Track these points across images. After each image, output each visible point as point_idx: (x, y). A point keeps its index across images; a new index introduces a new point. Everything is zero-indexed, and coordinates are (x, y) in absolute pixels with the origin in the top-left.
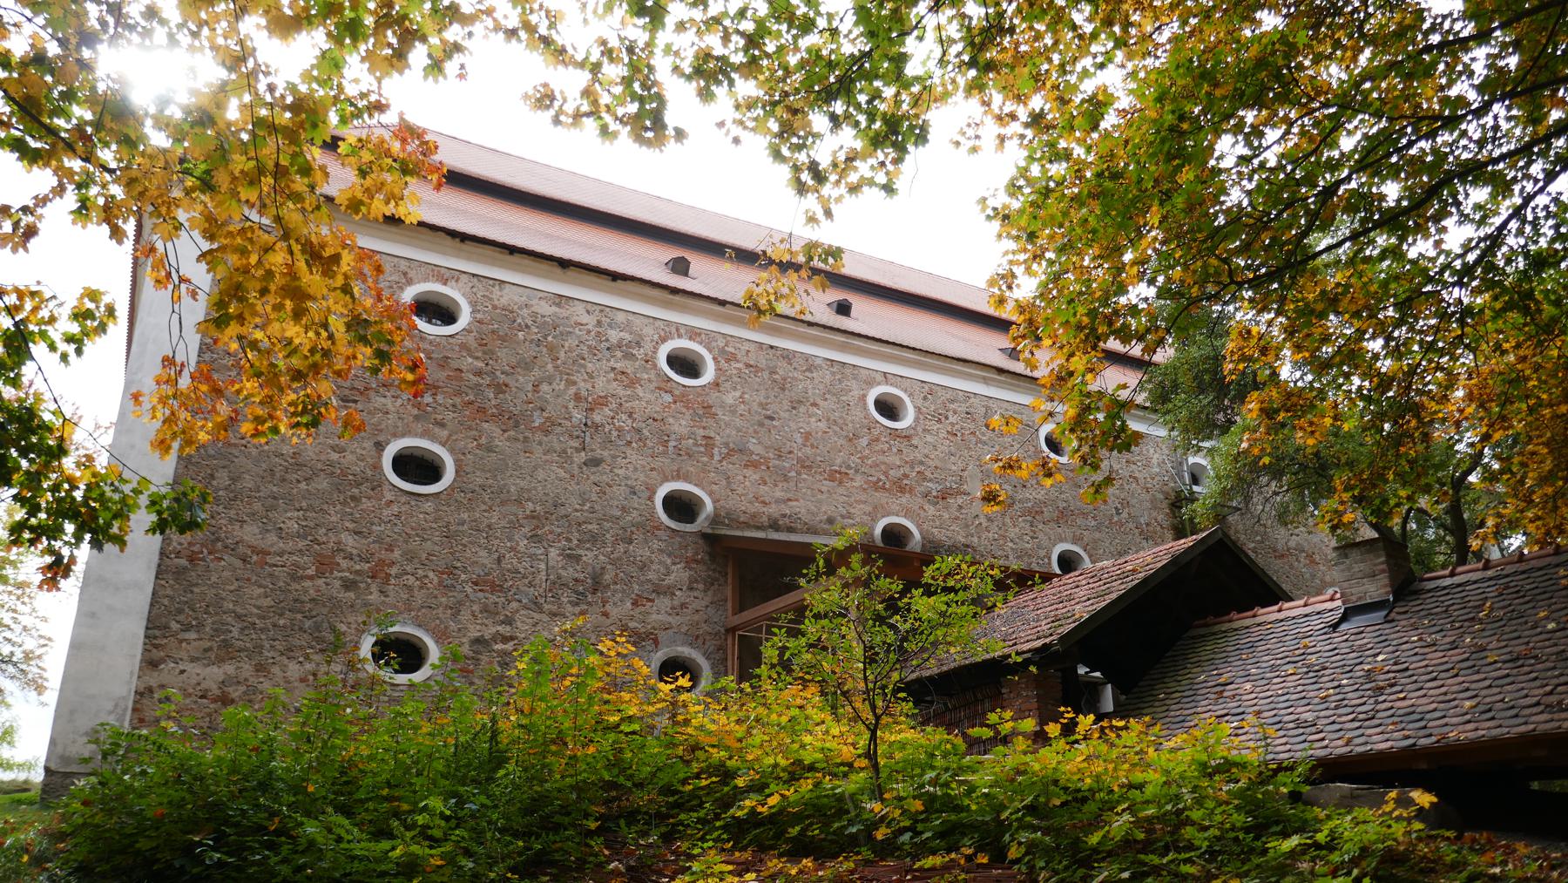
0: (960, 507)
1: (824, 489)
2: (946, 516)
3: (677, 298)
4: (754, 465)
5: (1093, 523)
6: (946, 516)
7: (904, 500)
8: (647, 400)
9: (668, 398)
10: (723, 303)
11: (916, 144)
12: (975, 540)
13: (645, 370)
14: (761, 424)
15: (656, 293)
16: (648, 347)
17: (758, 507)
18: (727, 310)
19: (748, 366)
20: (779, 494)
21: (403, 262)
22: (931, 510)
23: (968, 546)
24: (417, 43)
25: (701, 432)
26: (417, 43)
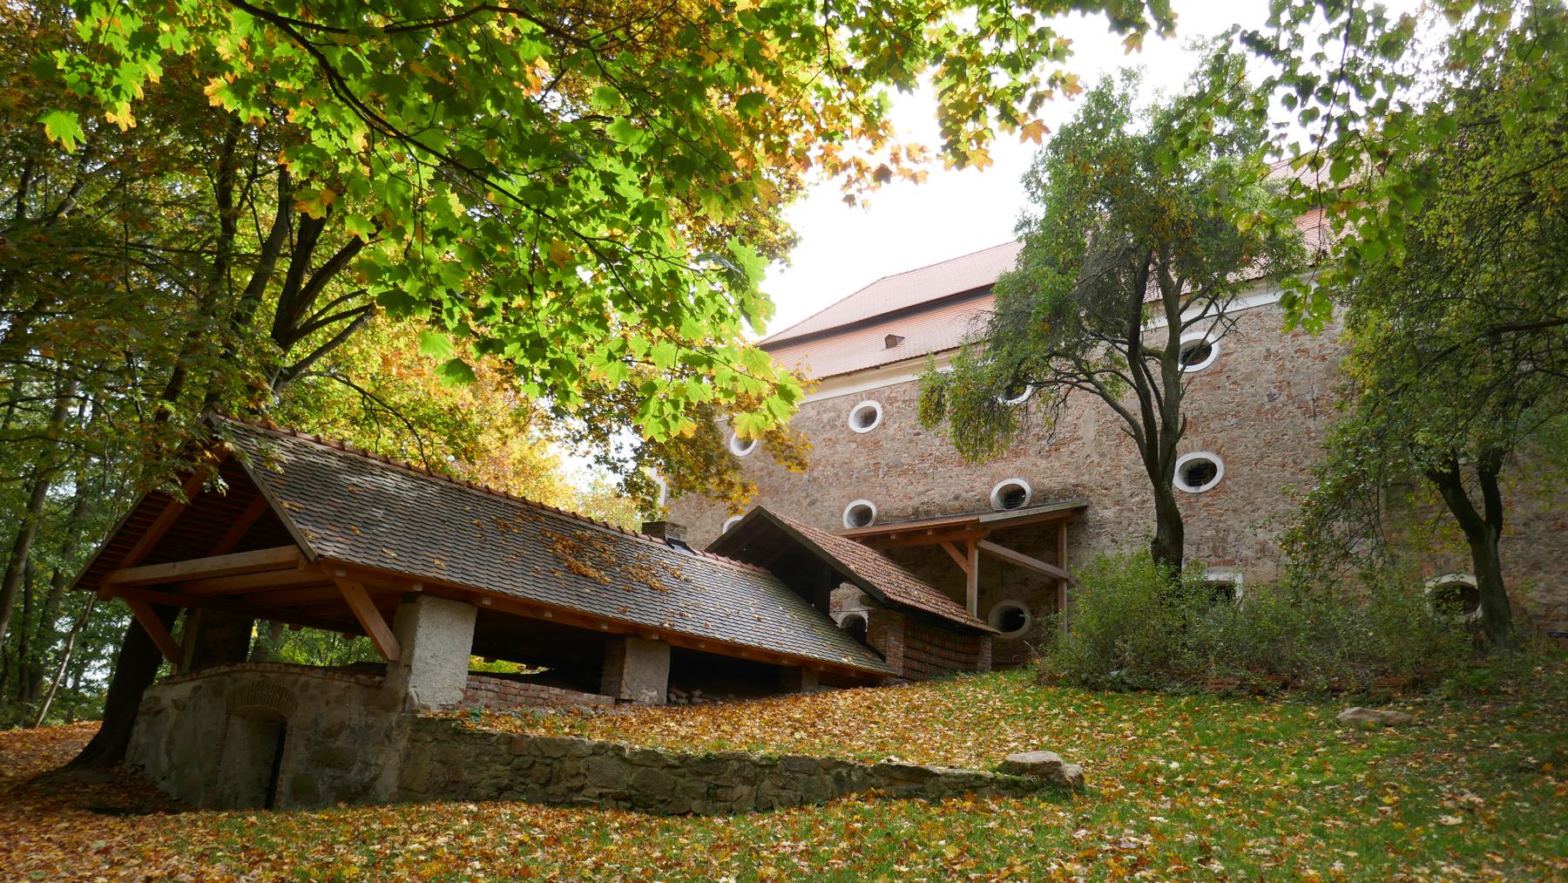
0: (1072, 452)
1: (953, 474)
2: (1057, 464)
3: (853, 377)
4: (904, 473)
5: (1234, 421)
6: (1057, 464)
7: (1018, 463)
8: (844, 450)
9: (854, 445)
10: (877, 367)
11: (1088, 106)
12: (1086, 478)
13: (842, 432)
14: (911, 441)
15: (841, 379)
16: (843, 416)
17: (907, 502)
18: (883, 370)
19: (904, 402)
20: (921, 488)
21: (1263, 309)
22: (1043, 464)
23: (1077, 486)
24: (1103, 12)
25: (872, 461)
26: (1103, 12)
